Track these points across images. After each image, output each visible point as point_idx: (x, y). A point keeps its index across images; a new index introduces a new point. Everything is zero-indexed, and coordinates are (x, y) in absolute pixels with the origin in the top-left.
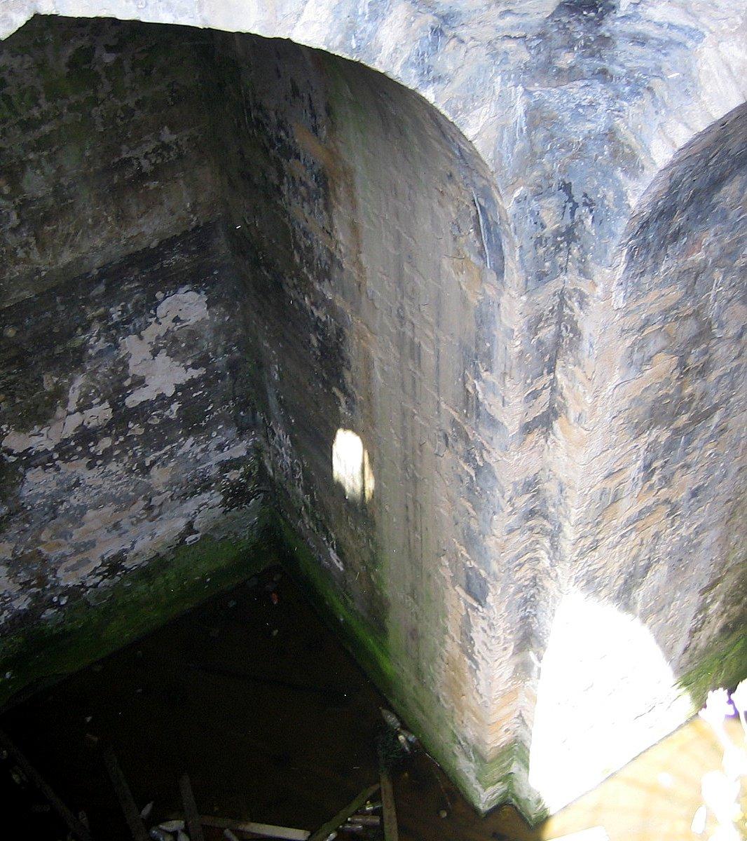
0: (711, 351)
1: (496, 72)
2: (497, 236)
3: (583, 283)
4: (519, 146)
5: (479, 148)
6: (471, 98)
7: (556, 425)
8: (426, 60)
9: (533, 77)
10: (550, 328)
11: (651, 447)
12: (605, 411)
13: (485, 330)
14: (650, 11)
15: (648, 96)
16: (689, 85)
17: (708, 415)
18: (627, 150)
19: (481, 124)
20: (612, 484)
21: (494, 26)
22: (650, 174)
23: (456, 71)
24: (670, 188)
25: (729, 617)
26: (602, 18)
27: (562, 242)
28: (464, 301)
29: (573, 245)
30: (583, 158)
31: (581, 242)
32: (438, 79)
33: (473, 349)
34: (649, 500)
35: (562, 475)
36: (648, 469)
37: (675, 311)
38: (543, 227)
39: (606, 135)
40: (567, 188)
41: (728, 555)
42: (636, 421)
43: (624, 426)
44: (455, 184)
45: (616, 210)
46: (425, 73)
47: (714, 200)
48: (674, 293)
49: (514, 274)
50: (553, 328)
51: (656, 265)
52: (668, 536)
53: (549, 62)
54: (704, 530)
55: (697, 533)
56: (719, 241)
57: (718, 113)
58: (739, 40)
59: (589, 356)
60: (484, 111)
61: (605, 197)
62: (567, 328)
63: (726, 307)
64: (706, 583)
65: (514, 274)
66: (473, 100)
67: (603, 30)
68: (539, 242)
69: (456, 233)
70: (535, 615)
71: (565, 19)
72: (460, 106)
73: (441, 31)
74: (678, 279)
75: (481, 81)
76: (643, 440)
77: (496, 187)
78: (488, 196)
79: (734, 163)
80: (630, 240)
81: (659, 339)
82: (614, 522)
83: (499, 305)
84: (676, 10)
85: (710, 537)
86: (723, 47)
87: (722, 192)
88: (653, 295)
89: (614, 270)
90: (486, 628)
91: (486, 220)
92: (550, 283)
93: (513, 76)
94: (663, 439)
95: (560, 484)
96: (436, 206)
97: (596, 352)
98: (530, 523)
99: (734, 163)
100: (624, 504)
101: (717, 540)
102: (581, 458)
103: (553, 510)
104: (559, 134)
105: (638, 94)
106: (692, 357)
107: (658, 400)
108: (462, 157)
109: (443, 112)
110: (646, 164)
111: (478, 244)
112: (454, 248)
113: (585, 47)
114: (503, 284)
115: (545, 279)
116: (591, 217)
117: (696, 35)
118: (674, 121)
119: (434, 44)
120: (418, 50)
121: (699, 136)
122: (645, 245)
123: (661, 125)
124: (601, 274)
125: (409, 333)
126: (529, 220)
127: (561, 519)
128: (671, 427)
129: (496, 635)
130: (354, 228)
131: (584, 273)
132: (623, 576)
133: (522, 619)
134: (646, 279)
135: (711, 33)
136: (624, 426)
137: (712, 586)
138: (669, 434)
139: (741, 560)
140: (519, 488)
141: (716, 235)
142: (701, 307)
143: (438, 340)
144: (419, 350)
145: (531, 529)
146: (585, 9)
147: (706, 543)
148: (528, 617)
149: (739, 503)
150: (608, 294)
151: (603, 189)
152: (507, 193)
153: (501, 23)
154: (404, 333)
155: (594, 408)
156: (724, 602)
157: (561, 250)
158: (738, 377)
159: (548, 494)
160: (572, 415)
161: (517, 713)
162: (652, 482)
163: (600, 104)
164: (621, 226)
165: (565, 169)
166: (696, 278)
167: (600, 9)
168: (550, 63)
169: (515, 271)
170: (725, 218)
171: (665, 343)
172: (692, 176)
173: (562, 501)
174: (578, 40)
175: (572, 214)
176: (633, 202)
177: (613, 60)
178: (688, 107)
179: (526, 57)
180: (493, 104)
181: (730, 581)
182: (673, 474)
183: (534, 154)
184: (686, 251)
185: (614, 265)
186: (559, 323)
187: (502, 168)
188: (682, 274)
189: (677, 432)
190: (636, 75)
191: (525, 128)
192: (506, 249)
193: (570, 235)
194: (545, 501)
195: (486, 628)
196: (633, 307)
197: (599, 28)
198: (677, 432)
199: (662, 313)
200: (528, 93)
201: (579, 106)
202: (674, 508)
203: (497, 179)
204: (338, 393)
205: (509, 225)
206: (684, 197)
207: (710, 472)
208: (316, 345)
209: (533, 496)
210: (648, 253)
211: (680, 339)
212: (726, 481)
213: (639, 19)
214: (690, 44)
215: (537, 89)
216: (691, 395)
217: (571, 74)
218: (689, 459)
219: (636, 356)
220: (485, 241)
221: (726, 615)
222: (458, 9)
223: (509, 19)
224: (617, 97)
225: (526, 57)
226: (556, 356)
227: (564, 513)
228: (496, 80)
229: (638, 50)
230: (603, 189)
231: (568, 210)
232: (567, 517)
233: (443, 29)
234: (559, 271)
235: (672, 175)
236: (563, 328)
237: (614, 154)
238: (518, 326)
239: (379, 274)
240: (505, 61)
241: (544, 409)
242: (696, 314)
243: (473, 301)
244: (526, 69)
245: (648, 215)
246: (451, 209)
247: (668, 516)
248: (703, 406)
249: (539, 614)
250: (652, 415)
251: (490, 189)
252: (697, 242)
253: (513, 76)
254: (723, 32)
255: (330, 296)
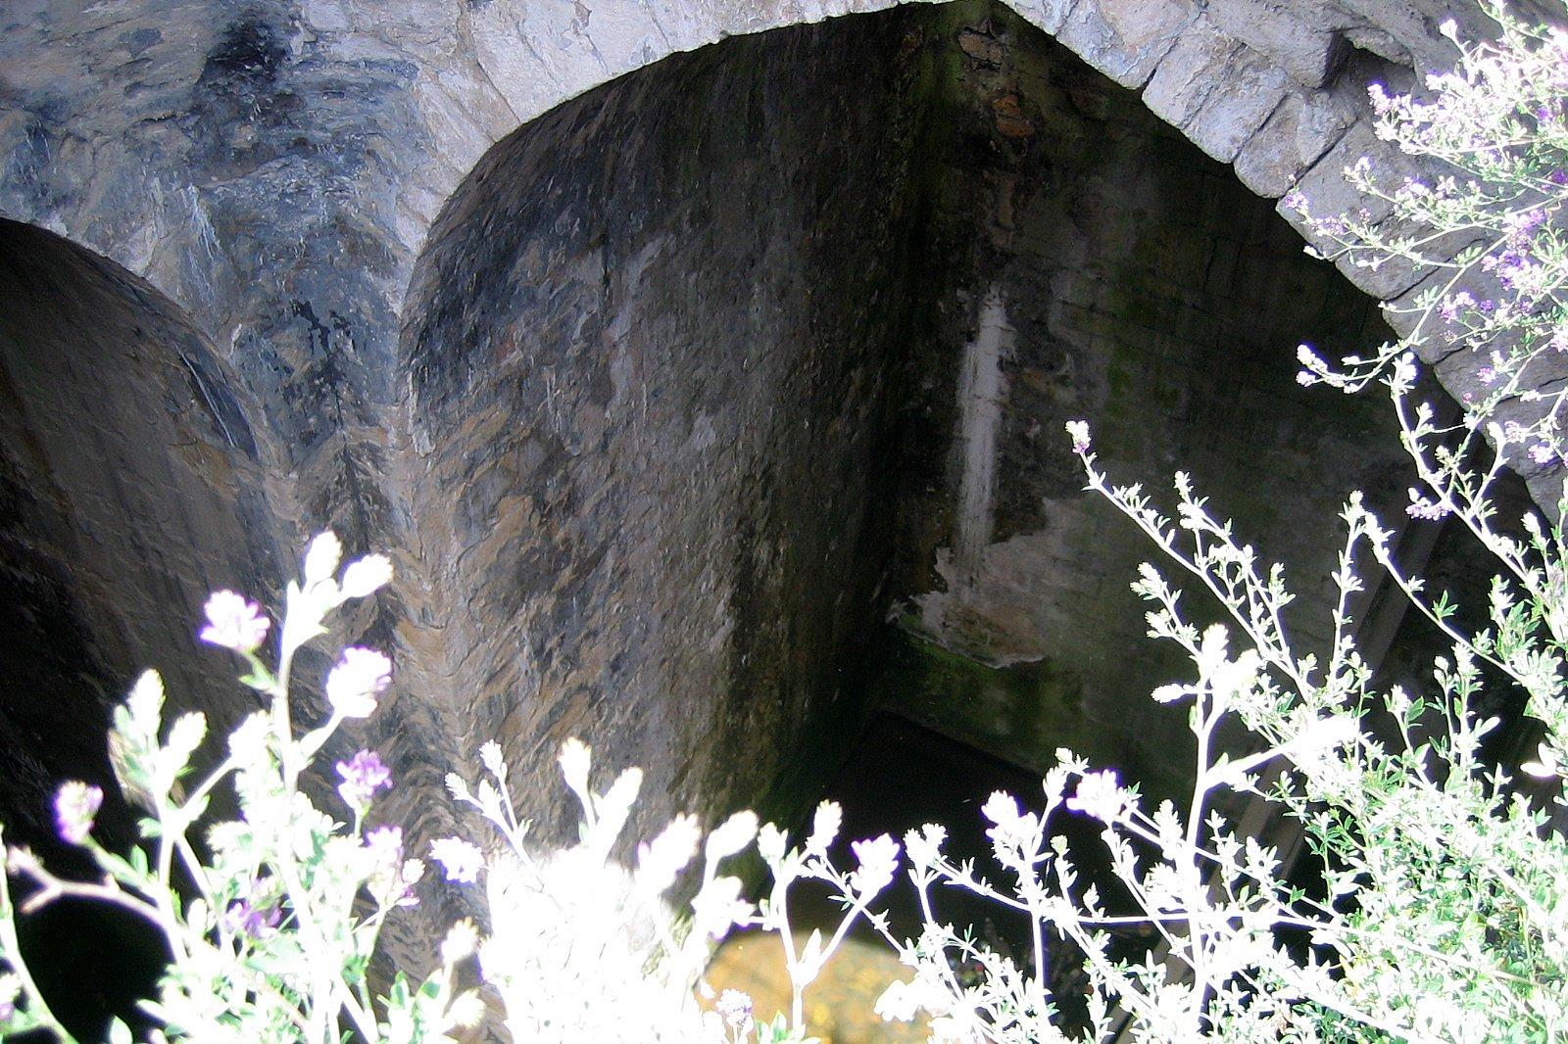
0: (573, 476)
1: (148, 173)
2: (229, 399)
3: (368, 434)
4: (217, 269)
5: (159, 285)
6: (123, 216)
7: (397, 633)
8: (35, 177)
9: (206, 169)
10: (345, 506)
11: (536, 623)
12: (456, 594)
13: (256, 532)
14: (334, 48)
15: (371, 163)
16: (417, 136)
17: (597, 560)
18: (368, 241)
19: (150, 251)
20: (498, 689)
21: (123, 109)
22: (407, 265)
23: (87, 183)
24: (442, 277)
25: (716, 808)
26: (272, 70)
27: (322, 385)
28: (217, 502)
29: (339, 385)
30: (313, 266)
31: (349, 378)
32: (62, 200)
33: (251, 564)
34: (558, 694)
35: (429, 697)
36: (542, 655)
37: (507, 438)
38: (289, 371)
39: (334, 226)
40: (305, 310)
41: (687, 731)
42: (503, 596)
43: (488, 608)
44: (150, 343)
45: (379, 324)
46: (40, 195)
47: (510, 280)
48: (498, 414)
49: (270, 447)
50: (349, 505)
51: (460, 384)
52: (600, 731)
53: (221, 144)
54: (644, 709)
55: (637, 716)
56: (535, 330)
57: (466, 167)
58: (460, 65)
59: (408, 528)
60: (148, 233)
61: (359, 310)
62: (368, 499)
63: (573, 413)
64: (671, 776)
65: (270, 447)
66: (126, 220)
67: (280, 86)
68: (290, 393)
69: (173, 410)
70: (461, 895)
71: (222, 81)
72: (110, 232)
73: (45, 132)
74: (496, 394)
75: (130, 190)
76: (521, 619)
77: (203, 334)
78: (199, 350)
79: (520, 225)
80: (411, 360)
81: (497, 480)
82: (520, 737)
83: (263, 494)
84: (368, 41)
85: (655, 717)
86: (443, 78)
87: (518, 268)
88: (468, 426)
89: (403, 404)
90: (401, 935)
91: (207, 382)
92: (324, 446)
93: (175, 174)
94: (548, 609)
95: (430, 710)
96: (133, 379)
97: (415, 520)
98: (408, 775)
99: (520, 225)
100: (526, 708)
101: (666, 716)
102: (444, 667)
103: (433, 748)
104: (269, 239)
105: (358, 162)
106: (550, 490)
107: (523, 561)
108: (143, 303)
109: (87, 245)
110: (398, 253)
111: (208, 418)
112: (179, 432)
113: (264, 113)
114: (259, 463)
115: (316, 441)
116: (350, 343)
117: (405, 69)
118: (414, 188)
119: (39, 152)
120: (16, 164)
121: (453, 200)
122: (435, 361)
123: (399, 197)
124: (388, 414)
125: (157, 567)
126: (265, 367)
127: (448, 756)
128: (553, 590)
129: (417, 940)
130: (31, 439)
131: (366, 419)
132: (558, 803)
133: (444, 906)
134: (452, 405)
135: (424, 63)
136: (488, 608)
137: (681, 776)
138: (554, 599)
139: (707, 731)
140: (376, 733)
141: (528, 324)
142: (539, 424)
143: (200, 566)
144: (180, 588)
145: (414, 782)
146: (246, 62)
147: (653, 724)
148: (452, 901)
149: (678, 660)
150: (405, 440)
151: (353, 300)
152: (220, 338)
153: (131, 103)
154: (150, 567)
155: (438, 596)
156: (704, 792)
157: (324, 396)
158: (620, 499)
159: (419, 729)
160: (414, 614)
161: (486, 1032)
162: (553, 668)
163: (312, 187)
164: (392, 344)
165: (295, 286)
166: (520, 388)
167: (266, 59)
168: (223, 145)
169: (268, 442)
170: (533, 299)
171: (507, 483)
172: (467, 254)
173: (440, 731)
174: (251, 107)
175: (325, 343)
176: (397, 308)
177: (308, 123)
178: (425, 167)
179: (186, 143)
180: (158, 218)
181: (702, 762)
182: (577, 650)
183: (241, 275)
184: (496, 355)
185: (401, 399)
186: (355, 495)
187: (202, 305)
188: (499, 386)
189: (563, 593)
190: (347, 137)
191: (217, 243)
192: (246, 413)
193: (330, 372)
194: (418, 739)
195: (401, 935)
196: (447, 447)
197: (274, 85)
198: (563, 593)
199: (489, 444)
200: (205, 192)
201: (284, 195)
202: (595, 695)
203: (198, 322)
204: (89, 680)
205: (239, 381)
206: (467, 284)
207: (625, 633)
208: (34, 620)
209: (400, 738)
210: (442, 370)
211: (526, 472)
212: (651, 637)
213: (324, 61)
214: (402, 82)
215: (215, 183)
216: (566, 541)
217: (257, 155)
218: (592, 624)
219: (472, 512)
220: (216, 410)
221: (711, 807)
222: (59, 95)
223: (142, 96)
224: (331, 171)
225: (186, 143)
226: (367, 540)
227: (447, 746)
228: (152, 185)
229: (337, 104)
230: (353, 300)
231: (317, 341)
232: (454, 752)
233: (48, 128)
234: (332, 424)
235: (437, 261)
236: (363, 501)
237: (353, 250)
238: (298, 515)
239: (88, 495)
240: (156, 155)
241: (375, 617)
242: (536, 433)
243: (228, 496)
244: (192, 160)
245: (424, 320)
246: (156, 378)
247: (590, 706)
248: (586, 550)
249: (464, 892)
250: (522, 582)
251: (195, 338)
252: (505, 339)
253: (175, 174)
254: (437, 59)
255: (29, 545)
